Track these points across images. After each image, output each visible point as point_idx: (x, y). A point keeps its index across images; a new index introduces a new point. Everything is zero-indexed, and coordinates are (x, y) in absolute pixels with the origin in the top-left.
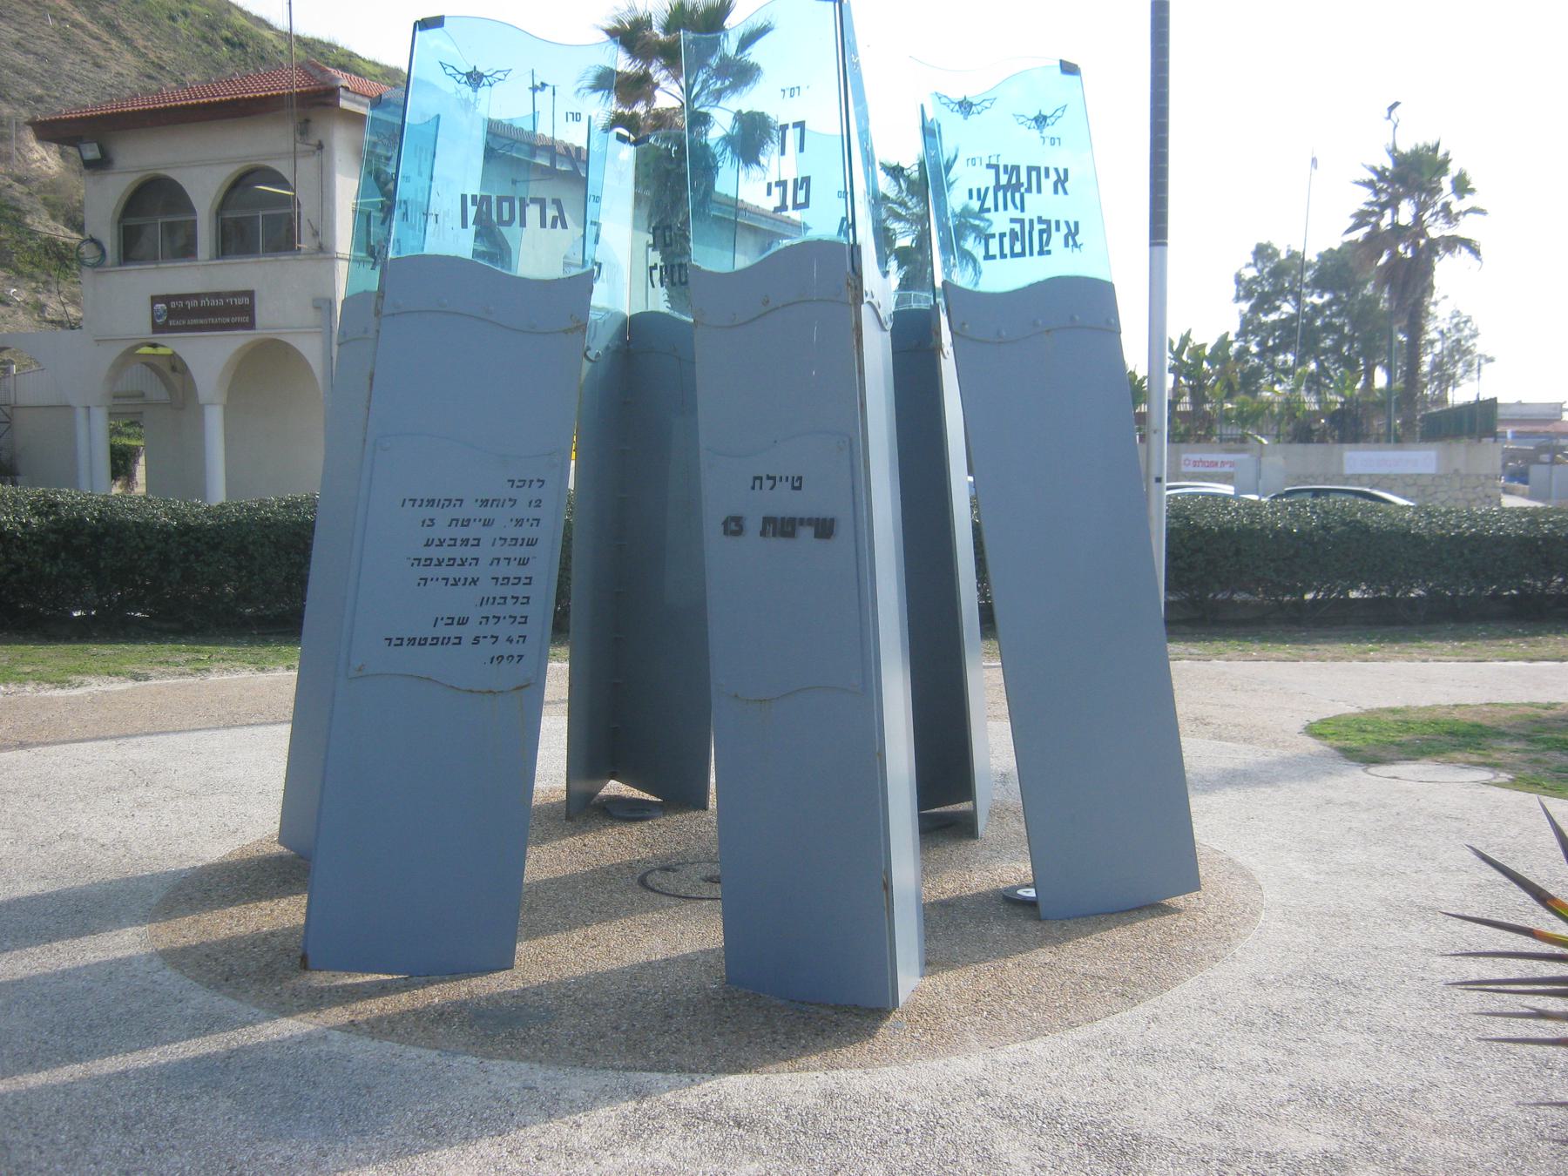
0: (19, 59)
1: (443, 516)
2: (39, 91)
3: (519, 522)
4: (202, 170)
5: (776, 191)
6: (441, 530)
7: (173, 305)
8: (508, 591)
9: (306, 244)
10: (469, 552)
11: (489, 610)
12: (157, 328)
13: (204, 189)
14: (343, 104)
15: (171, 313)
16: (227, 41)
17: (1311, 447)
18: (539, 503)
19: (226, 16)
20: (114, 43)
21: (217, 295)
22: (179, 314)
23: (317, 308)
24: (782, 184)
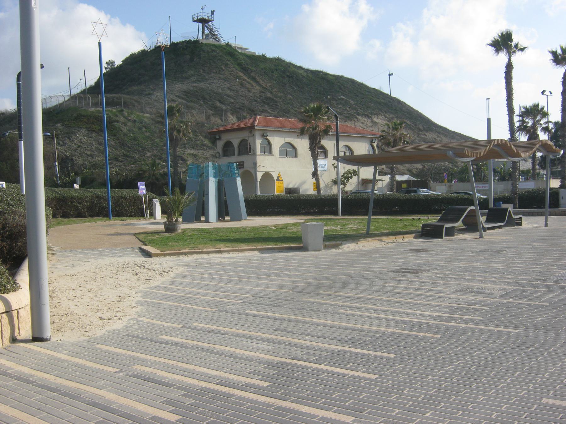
0: (229, 92)
2: (233, 101)
13: (236, 143)
17: (465, 183)
20: (254, 84)
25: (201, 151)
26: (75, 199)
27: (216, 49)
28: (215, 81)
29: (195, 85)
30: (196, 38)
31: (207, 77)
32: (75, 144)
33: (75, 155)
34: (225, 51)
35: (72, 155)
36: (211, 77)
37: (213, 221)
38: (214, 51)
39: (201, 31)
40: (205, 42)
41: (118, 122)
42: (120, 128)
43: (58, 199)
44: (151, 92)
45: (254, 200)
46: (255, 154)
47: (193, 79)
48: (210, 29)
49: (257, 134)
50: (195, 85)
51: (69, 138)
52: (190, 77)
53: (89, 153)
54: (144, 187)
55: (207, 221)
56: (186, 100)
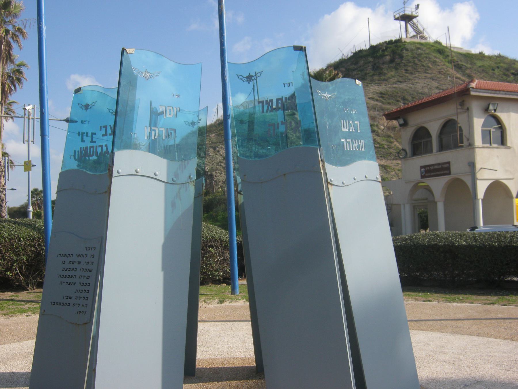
1: (68, 260)
3: (88, 263)
4: (433, 122)
5: (104, 130)
6: (67, 266)
7: (426, 169)
8: (83, 288)
9: (465, 143)
10: (72, 273)
11: (78, 294)
12: (423, 177)
13: (434, 128)
14: (472, 93)
15: (426, 172)
16: (513, 74)
18: (93, 256)
19: (513, 65)
21: (439, 164)
22: (429, 172)
23: (469, 165)
24: (106, 127)
25: (395, 162)
27: (423, 47)
28: (420, 81)
29: (394, 86)
31: (410, 77)
33: (217, 169)
34: (432, 48)
35: (212, 170)
36: (415, 77)
38: (418, 48)
39: (403, 30)
40: (408, 40)
45: (470, 247)
46: (471, 145)
47: (392, 80)
49: (475, 107)
50: (394, 86)
56: (382, 102)
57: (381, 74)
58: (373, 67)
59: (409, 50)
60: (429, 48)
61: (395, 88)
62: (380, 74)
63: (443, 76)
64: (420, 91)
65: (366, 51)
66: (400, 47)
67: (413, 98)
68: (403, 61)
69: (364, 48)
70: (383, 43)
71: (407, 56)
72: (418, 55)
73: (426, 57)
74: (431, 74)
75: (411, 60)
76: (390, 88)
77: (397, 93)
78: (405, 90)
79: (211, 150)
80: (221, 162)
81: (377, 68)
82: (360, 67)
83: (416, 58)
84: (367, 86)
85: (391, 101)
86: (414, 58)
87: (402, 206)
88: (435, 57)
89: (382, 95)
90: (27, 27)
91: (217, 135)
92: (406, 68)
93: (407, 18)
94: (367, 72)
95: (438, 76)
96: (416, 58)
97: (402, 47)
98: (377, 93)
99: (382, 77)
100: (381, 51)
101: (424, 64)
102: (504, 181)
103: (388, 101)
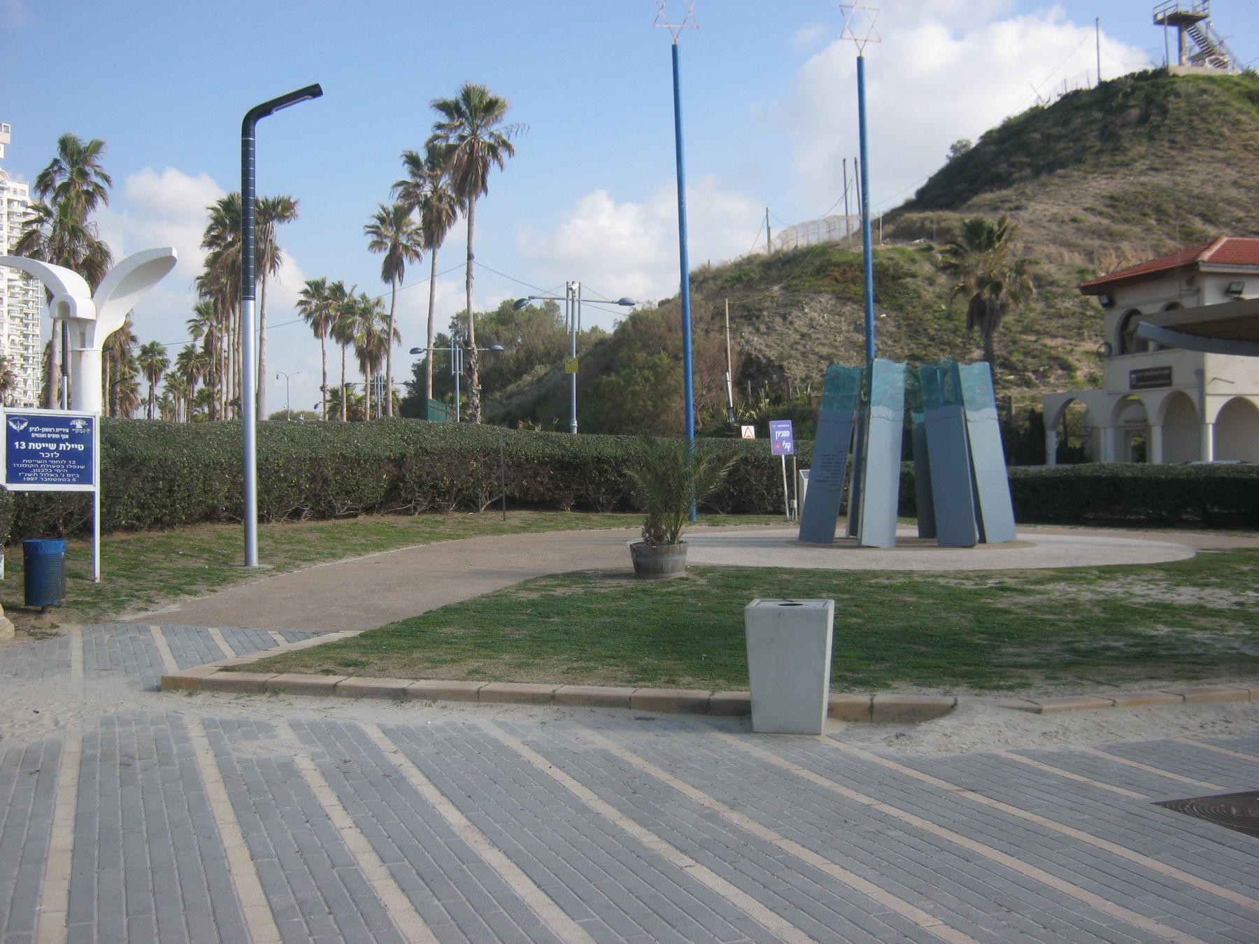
0: (1234, 193)
2: (1241, 214)
12: (1133, 387)
15: (1140, 379)
21: (1156, 369)
22: (1143, 379)
26: (609, 463)
27: (1213, 87)
28: (1200, 167)
29: (1143, 179)
30: (1160, 65)
32: (796, 330)
33: (790, 357)
34: (1237, 89)
35: (781, 357)
36: (1190, 158)
37: (883, 544)
38: (1204, 91)
40: (1181, 72)
41: (914, 276)
42: (915, 291)
43: (559, 461)
44: (1024, 202)
45: (1135, 479)
47: (1140, 166)
48: (1201, 40)
50: (1143, 179)
51: (784, 318)
52: (1135, 161)
53: (824, 351)
54: (787, 434)
55: (854, 539)
57: (1117, 149)
58: (1102, 134)
59: (1183, 94)
60: (1228, 90)
61: (1143, 184)
62: (1116, 149)
63: (1251, 156)
64: (1196, 191)
65: (1089, 93)
66: (1163, 87)
67: (1178, 207)
68: (1167, 122)
69: (1084, 85)
70: (1126, 77)
71: (1177, 109)
72: (1201, 107)
73: (1219, 113)
74: (1225, 150)
75: (1185, 118)
76: (1132, 184)
77: (1146, 197)
78: (1164, 190)
79: (778, 319)
80: (797, 343)
81: (1109, 136)
82: (1074, 131)
83: (1196, 114)
84: (1085, 178)
85: (1131, 215)
86: (1191, 114)
87: (1102, 431)
88: (1240, 111)
89: (1113, 200)
90: (513, 135)
91: (784, 288)
92: (1172, 136)
93: (1182, 21)
94: (1088, 144)
95: (1240, 155)
96: (1196, 114)
97: (1168, 88)
98: (1103, 197)
99: (1119, 158)
100: (1120, 95)
101: (1213, 129)
102: (1252, 399)
103: (1124, 214)
